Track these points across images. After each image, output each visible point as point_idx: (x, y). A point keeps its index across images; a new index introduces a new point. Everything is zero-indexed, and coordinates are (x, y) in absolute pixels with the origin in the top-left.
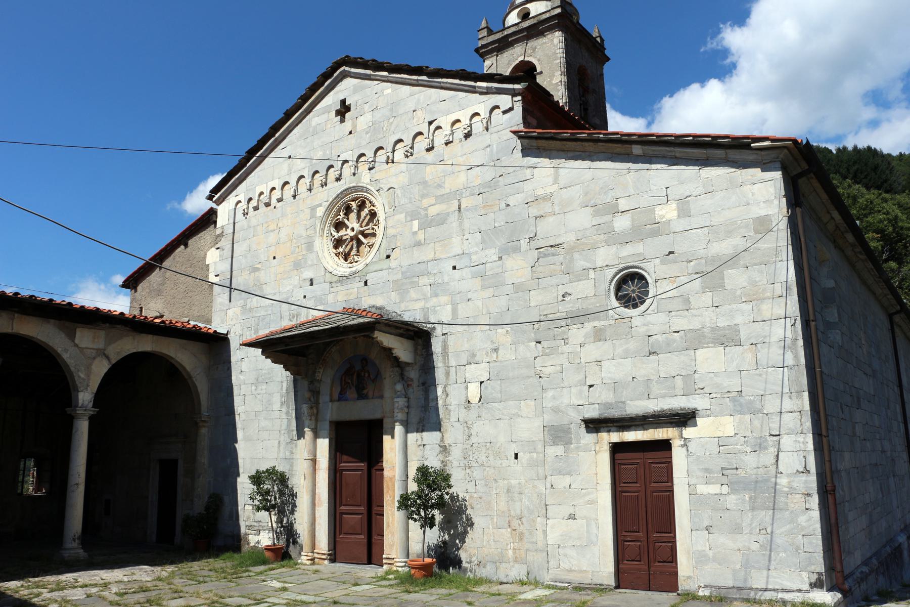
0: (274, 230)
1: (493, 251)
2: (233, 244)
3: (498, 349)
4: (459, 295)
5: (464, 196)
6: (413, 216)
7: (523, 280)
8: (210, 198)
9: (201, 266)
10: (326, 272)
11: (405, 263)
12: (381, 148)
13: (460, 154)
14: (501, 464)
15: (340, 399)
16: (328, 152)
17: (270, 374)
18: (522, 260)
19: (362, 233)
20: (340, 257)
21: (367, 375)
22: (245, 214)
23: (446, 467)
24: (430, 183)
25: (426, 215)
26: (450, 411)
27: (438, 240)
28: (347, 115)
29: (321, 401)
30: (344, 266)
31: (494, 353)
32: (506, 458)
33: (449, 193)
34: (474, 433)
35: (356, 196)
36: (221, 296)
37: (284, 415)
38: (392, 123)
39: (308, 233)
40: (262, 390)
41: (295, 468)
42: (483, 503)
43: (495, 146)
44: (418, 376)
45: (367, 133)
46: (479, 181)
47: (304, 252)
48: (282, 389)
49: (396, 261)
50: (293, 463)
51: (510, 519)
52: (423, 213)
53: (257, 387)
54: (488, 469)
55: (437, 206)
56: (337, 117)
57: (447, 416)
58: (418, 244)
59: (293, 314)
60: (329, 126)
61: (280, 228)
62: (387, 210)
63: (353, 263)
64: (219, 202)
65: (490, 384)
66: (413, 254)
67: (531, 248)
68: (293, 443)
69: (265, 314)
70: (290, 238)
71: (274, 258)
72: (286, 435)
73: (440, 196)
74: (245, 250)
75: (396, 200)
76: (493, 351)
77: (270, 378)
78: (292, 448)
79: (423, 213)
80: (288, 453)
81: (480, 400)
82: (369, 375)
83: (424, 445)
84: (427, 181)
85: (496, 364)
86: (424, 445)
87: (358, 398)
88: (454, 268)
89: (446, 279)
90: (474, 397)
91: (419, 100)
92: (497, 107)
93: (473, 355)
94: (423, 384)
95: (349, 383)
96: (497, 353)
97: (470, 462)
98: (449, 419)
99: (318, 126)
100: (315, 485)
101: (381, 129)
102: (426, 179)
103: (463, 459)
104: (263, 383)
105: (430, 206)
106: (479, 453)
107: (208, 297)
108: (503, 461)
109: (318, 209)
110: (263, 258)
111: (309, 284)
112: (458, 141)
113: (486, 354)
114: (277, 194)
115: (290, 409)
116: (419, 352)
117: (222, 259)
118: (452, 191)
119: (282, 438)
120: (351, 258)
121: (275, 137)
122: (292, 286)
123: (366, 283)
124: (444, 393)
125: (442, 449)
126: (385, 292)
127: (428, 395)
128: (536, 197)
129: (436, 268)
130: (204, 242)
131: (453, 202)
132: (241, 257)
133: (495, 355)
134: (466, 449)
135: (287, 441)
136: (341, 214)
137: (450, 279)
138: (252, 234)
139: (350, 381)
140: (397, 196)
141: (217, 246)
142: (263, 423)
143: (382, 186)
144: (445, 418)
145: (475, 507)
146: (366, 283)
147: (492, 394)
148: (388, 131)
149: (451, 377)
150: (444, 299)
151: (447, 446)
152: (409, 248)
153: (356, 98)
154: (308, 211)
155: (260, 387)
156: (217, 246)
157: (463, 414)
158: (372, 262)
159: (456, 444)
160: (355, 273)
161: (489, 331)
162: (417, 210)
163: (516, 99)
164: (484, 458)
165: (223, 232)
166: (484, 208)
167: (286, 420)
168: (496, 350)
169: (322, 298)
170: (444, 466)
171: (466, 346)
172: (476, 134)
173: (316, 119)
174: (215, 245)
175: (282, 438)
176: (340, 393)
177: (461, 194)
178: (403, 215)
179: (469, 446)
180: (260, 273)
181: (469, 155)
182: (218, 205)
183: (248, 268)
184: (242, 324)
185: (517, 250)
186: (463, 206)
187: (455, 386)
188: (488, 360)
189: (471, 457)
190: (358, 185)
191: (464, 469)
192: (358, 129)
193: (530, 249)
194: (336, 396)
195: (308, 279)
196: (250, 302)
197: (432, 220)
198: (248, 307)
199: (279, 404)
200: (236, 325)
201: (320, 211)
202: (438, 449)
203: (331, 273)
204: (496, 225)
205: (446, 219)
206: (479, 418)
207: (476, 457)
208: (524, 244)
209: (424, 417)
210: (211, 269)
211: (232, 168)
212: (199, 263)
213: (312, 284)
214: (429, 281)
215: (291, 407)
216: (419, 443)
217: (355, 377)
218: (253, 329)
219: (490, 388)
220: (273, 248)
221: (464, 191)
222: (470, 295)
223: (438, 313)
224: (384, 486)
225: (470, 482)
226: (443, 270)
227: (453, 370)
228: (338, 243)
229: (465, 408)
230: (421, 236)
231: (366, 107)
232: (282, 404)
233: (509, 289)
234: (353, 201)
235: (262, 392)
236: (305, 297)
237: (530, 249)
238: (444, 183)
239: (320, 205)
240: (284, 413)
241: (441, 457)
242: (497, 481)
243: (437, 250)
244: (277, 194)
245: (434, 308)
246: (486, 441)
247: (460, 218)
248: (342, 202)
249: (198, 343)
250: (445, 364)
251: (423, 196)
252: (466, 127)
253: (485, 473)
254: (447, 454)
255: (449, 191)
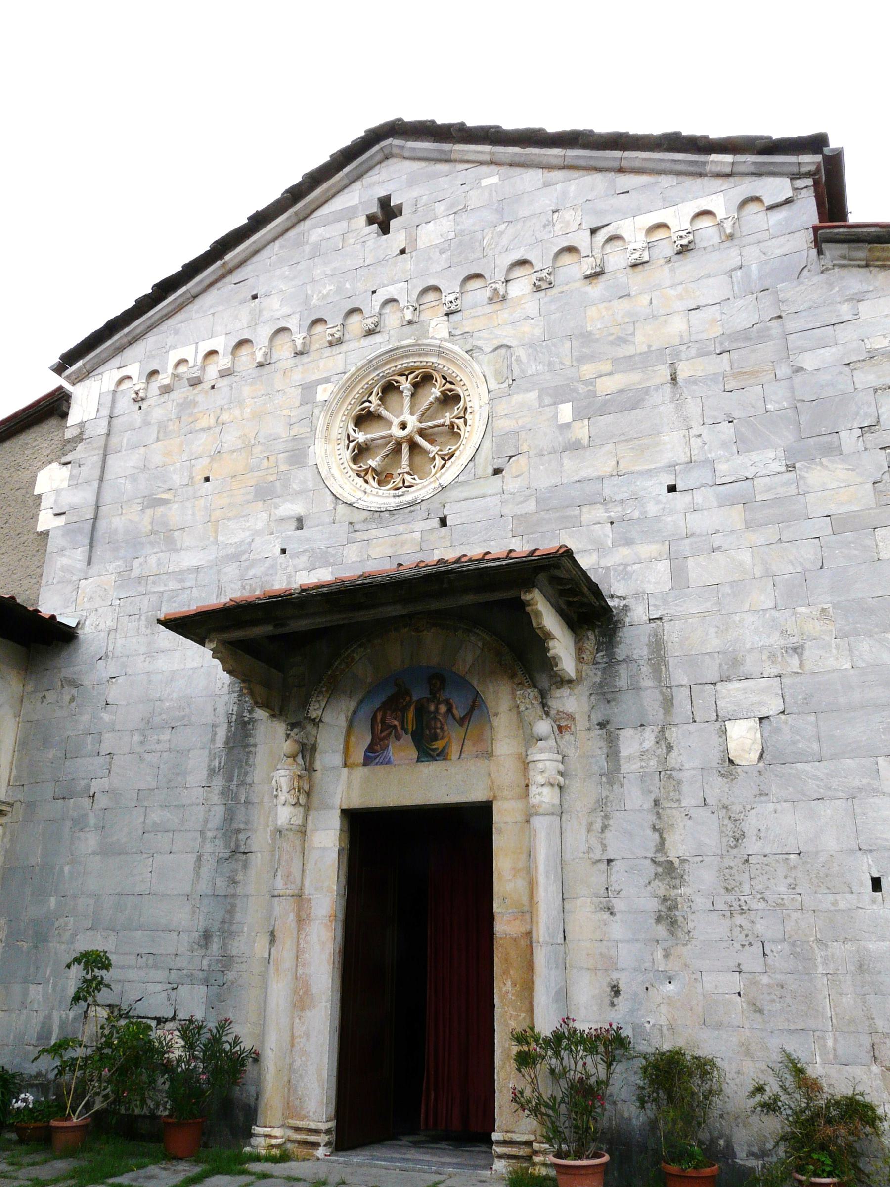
0: (209, 429)
1: (771, 454)
2: (105, 455)
3: (802, 646)
4: (687, 541)
5: (683, 356)
6: (559, 395)
7: (856, 508)
8: (59, 369)
9: (21, 498)
10: (336, 504)
11: (544, 481)
12: (478, 276)
13: (668, 283)
14: (835, 903)
15: (367, 761)
16: (348, 286)
17: (184, 709)
18: (846, 469)
19: (422, 433)
20: (369, 477)
21: (443, 709)
22: (138, 400)
23: (677, 913)
24: (597, 336)
25: (593, 394)
26: (679, 783)
27: (623, 438)
28: (393, 223)
29: (318, 765)
30: (373, 493)
31: (791, 656)
32: (847, 889)
33: (645, 353)
34: (750, 832)
35: (399, 367)
36: (67, 553)
37: (216, 798)
38: (502, 233)
39: (293, 433)
40: (159, 742)
41: (238, 917)
42: (788, 1000)
43: (754, 267)
44: (586, 708)
45: (442, 252)
46: (717, 331)
47: (283, 467)
48: (213, 740)
49: (519, 479)
50: (233, 906)
51: (877, 1040)
52: (582, 389)
53: (145, 737)
54: (795, 915)
55: (618, 377)
56: (398, 202)
57: (672, 794)
58: (575, 446)
59: (251, 585)
60: (352, 241)
61: (223, 424)
62: (493, 385)
63: (400, 488)
64: (76, 380)
65: (786, 722)
66: (562, 465)
67: (868, 446)
68: (237, 860)
69: (180, 587)
70: (250, 442)
71: (207, 479)
72: (219, 842)
73: (625, 357)
74: (134, 467)
75: (515, 366)
76: (790, 651)
77: (183, 717)
78: (235, 871)
79: (582, 389)
80: (221, 884)
81: (761, 756)
82: (450, 710)
83: (609, 861)
84: (590, 334)
85: (798, 679)
86: (609, 861)
87: (418, 758)
88: (672, 489)
89: (652, 509)
90: (743, 750)
91: (565, 194)
92: (757, 199)
93: (736, 662)
94: (602, 725)
95: (395, 726)
96: (800, 655)
97: (742, 898)
98: (679, 801)
99: (324, 243)
100: (532, 954)
101: (477, 244)
102: (589, 329)
103: (723, 891)
104: (163, 727)
105: (600, 376)
106: (766, 877)
107: (34, 556)
108: (838, 897)
109: (319, 387)
110: (177, 479)
111: (293, 528)
112: (662, 261)
113: (769, 657)
114: (223, 361)
115: (235, 782)
116: (587, 656)
117: (75, 483)
118: (652, 349)
119: (208, 847)
120: (398, 480)
121: (223, 261)
122: (247, 533)
123: (443, 522)
124: (662, 743)
125: (660, 870)
126: (493, 538)
127: (617, 746)
128: (869, 352)
129: (625, 489)
130: (33, 453)
131: (655, 369)
132: (122, 481)
133: (794, 661)
134: (731, 868)
135: (220, 856)
136: (372, 398)
137: (663, 509)
138: (154, 436)
139: (396, 723)
140: (518, 360)
141: (65, 459)
142: (156, 816)
143: (479, 343)
144: (667, 799)
145: (767, 1008)
146: (443, 522)
147: (794, 743)
148: (493, 246)
149: (677, 709)
150: (647, 550)
151: (677, 862)
152: (552, 455)
153: (415, 194)
154: (295, 394)
155: (155, 737)
156: (65, 459)
157: (716, 789)
158: (456, 483)
159: (700, 858)
160: (413, 504)
161: (773, 612)
162: (568, 385)
163: (800, 183)
164: (783, 889)
165: (81, 433)
166: (735, 378)
167: (223, 808)
168: (797, 650)
169: (327, 552)
170: (670, 909)
171: (714, 643)
172: (705, 248)
173: (320, 231)
174: (59, 457)
175: (208, 847)
176: (371, 749)
177: (676, 354)
178: (533, 395)
179: (738, 861)
180: (170, 509)
181: (692, 285)
182: (74, 384)
183: (139, 501)
184: (117, 608)
185: (833, 450)
186: (681, 376)
187: (692, 727)
188: (775, 671)
189: (746, 888)
190: (420, 342)
191: (728, 914)
192: (421, 244)
193: (866, 449)
194: (358, 755)
195: (290, 518)
196: (141, 564)
197: (605, 402)
198: (135, 573)
199: (205, 773)
200: (100, 610)
201: (325, 390)
202: (650, 869)
203: (350, 505)
204: (770, 407)
205: (643, 400)
206: (763, 798)
207: (759, 887)
208: (849, 439)
209: (607, 797)
210: (46, 503)
211: (119, 314)
212: (17, 493)
213: (300, 527)
214: (607, 515)
215: (235, 779)
216: (597, 854)
217: (411, 714)
218: (143, 618)
219: (786, 729)
220: (206, 461)
221: (684, 348)
222: (718, 540)
223: (634, 576)
224: (496, 959)
225: (747, 947)
226: (642, 493)
227: (681, 697)
228: (360, 452)
229: (722, 775)
230: (581, 431)
231: (440, 208)
232: (212, 772)
233: (823, 527)
234: (401, 375)
235: (159, 747)
236: (284, 551)
237: (866, 449)
238: (633, 334)
239: (327, 380)
240: (216, 792)
241: (660, 888)
242: (826, 945)
243: (624, 457)
244: (223, 361)
245: (625, 568)
246: (786, 850)
247: (677, 399)
248: (378, 375)
249: (12, 643)
250: (660, 681)
251: (582, 359)
252: (683, 234)
253: (790, 926)
254: (678, 881)
255: (646, 349)
